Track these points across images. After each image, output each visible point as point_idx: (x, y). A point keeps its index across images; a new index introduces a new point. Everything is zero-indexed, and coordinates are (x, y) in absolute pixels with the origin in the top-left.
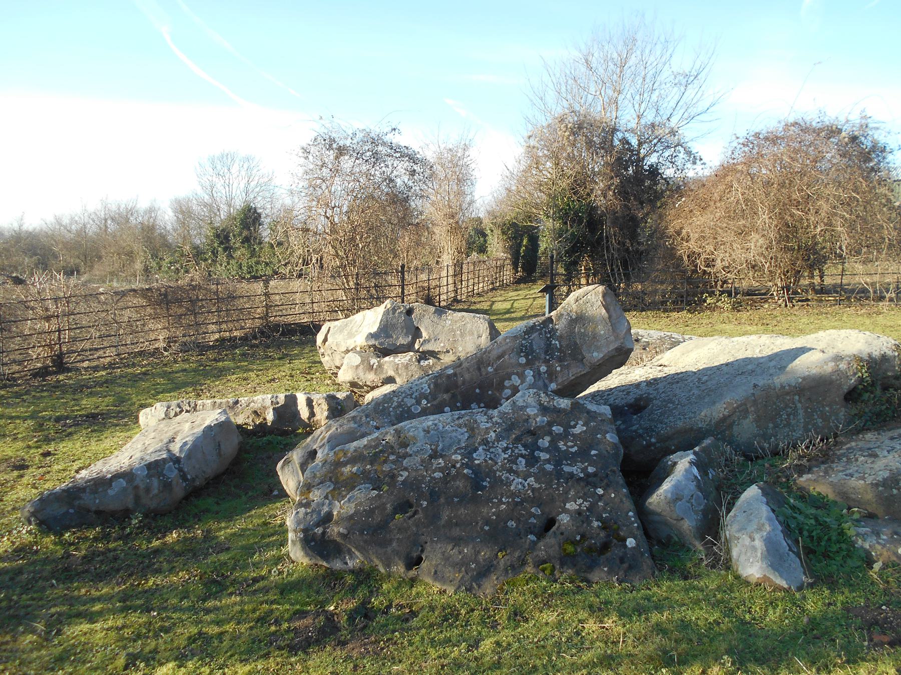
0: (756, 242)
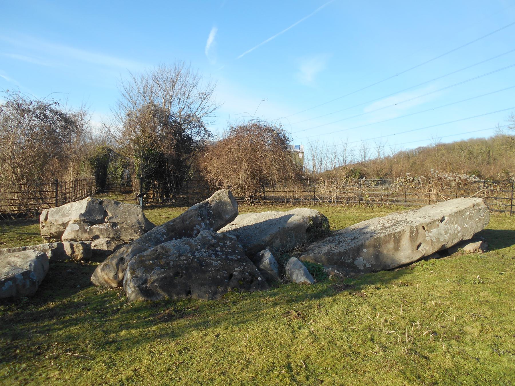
0: (242, 175)
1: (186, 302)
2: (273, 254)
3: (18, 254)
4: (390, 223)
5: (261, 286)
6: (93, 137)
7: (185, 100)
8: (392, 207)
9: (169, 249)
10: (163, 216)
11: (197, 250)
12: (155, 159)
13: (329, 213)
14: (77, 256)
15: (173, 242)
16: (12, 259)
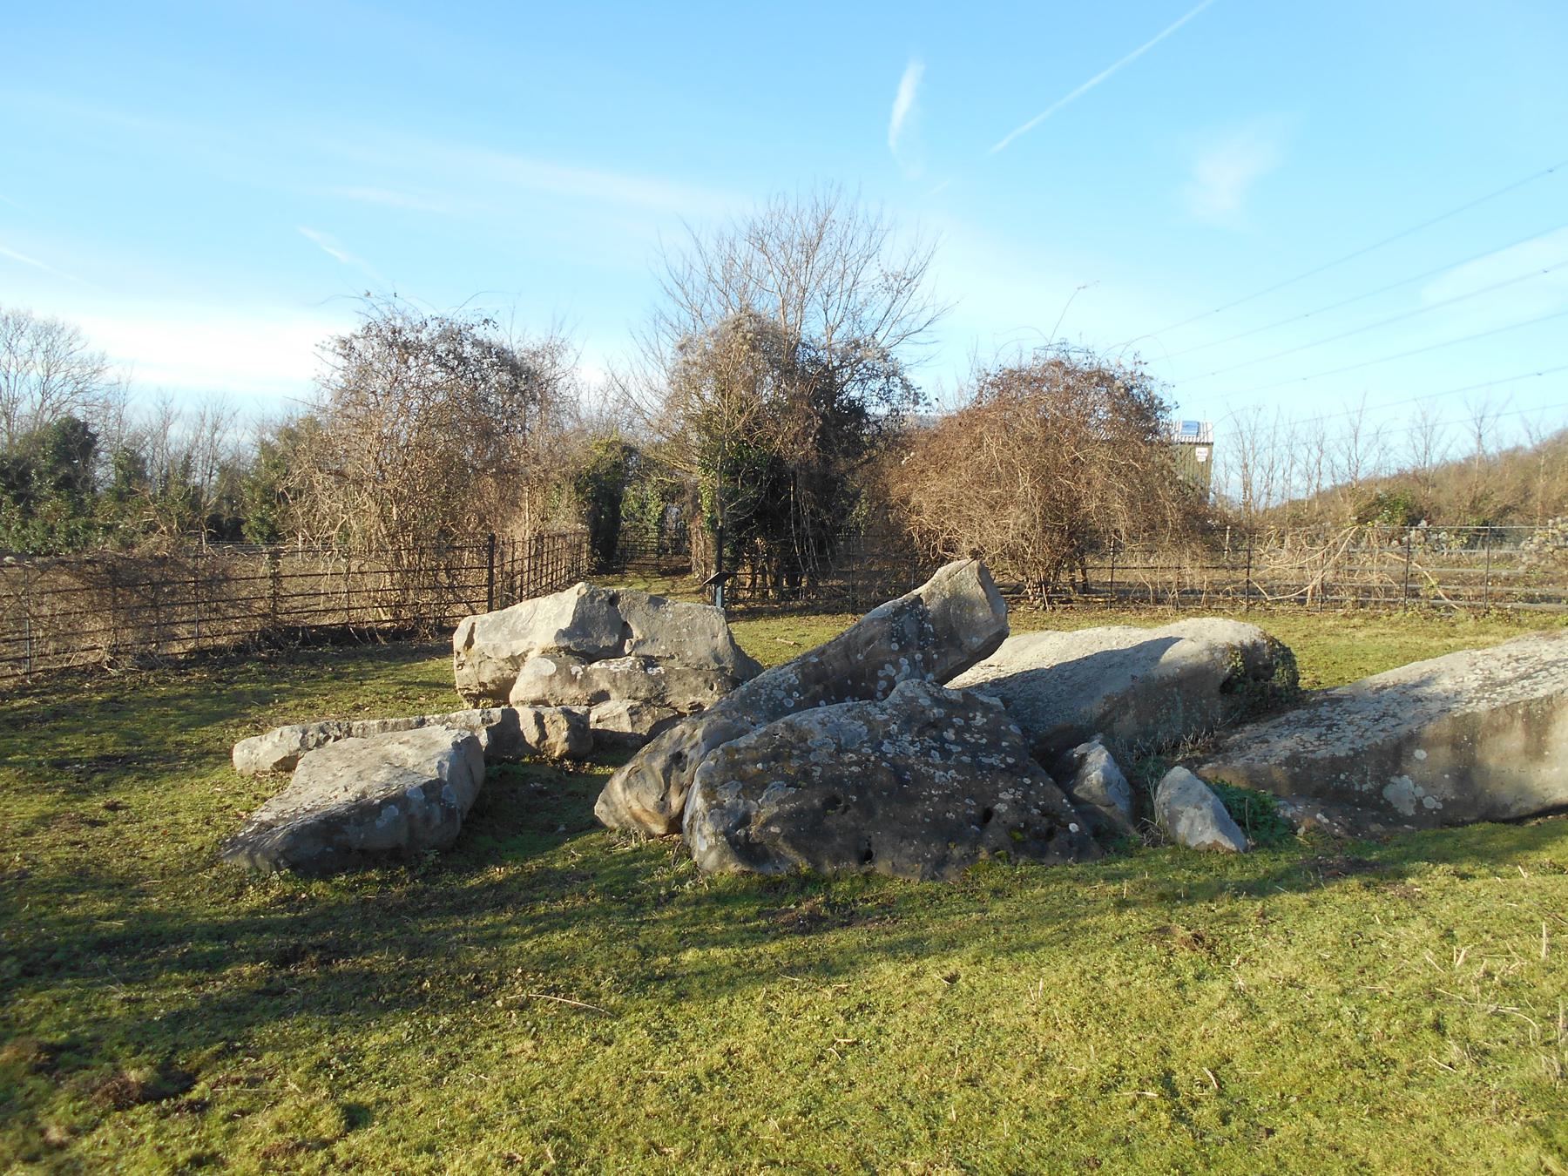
0: (1016, 518)
1: (858, 883)
2: (1116, 757)
3: (407, 735)
4: (1514, 670)
5: (1078, 849)
6: (583, 415)
7: (844, 298)
8: (1525, 619)
9: (810, 731)
10: (785, 641)
11: (888, 735)
12: (757, 474)
13: (1298, 635)
14: (552, 747)
15: (821, 712)
16: (394, 749)
